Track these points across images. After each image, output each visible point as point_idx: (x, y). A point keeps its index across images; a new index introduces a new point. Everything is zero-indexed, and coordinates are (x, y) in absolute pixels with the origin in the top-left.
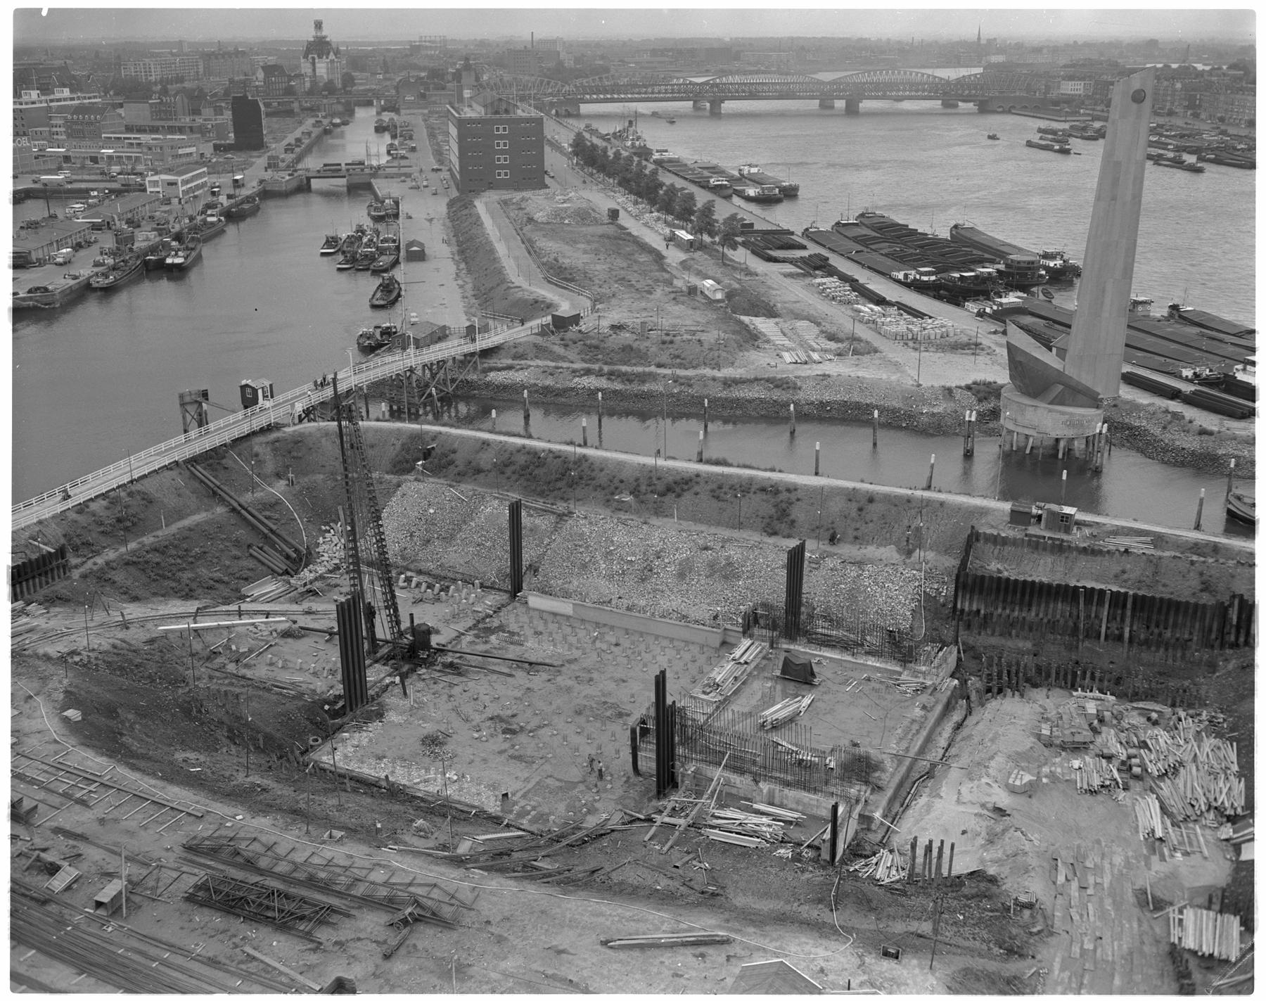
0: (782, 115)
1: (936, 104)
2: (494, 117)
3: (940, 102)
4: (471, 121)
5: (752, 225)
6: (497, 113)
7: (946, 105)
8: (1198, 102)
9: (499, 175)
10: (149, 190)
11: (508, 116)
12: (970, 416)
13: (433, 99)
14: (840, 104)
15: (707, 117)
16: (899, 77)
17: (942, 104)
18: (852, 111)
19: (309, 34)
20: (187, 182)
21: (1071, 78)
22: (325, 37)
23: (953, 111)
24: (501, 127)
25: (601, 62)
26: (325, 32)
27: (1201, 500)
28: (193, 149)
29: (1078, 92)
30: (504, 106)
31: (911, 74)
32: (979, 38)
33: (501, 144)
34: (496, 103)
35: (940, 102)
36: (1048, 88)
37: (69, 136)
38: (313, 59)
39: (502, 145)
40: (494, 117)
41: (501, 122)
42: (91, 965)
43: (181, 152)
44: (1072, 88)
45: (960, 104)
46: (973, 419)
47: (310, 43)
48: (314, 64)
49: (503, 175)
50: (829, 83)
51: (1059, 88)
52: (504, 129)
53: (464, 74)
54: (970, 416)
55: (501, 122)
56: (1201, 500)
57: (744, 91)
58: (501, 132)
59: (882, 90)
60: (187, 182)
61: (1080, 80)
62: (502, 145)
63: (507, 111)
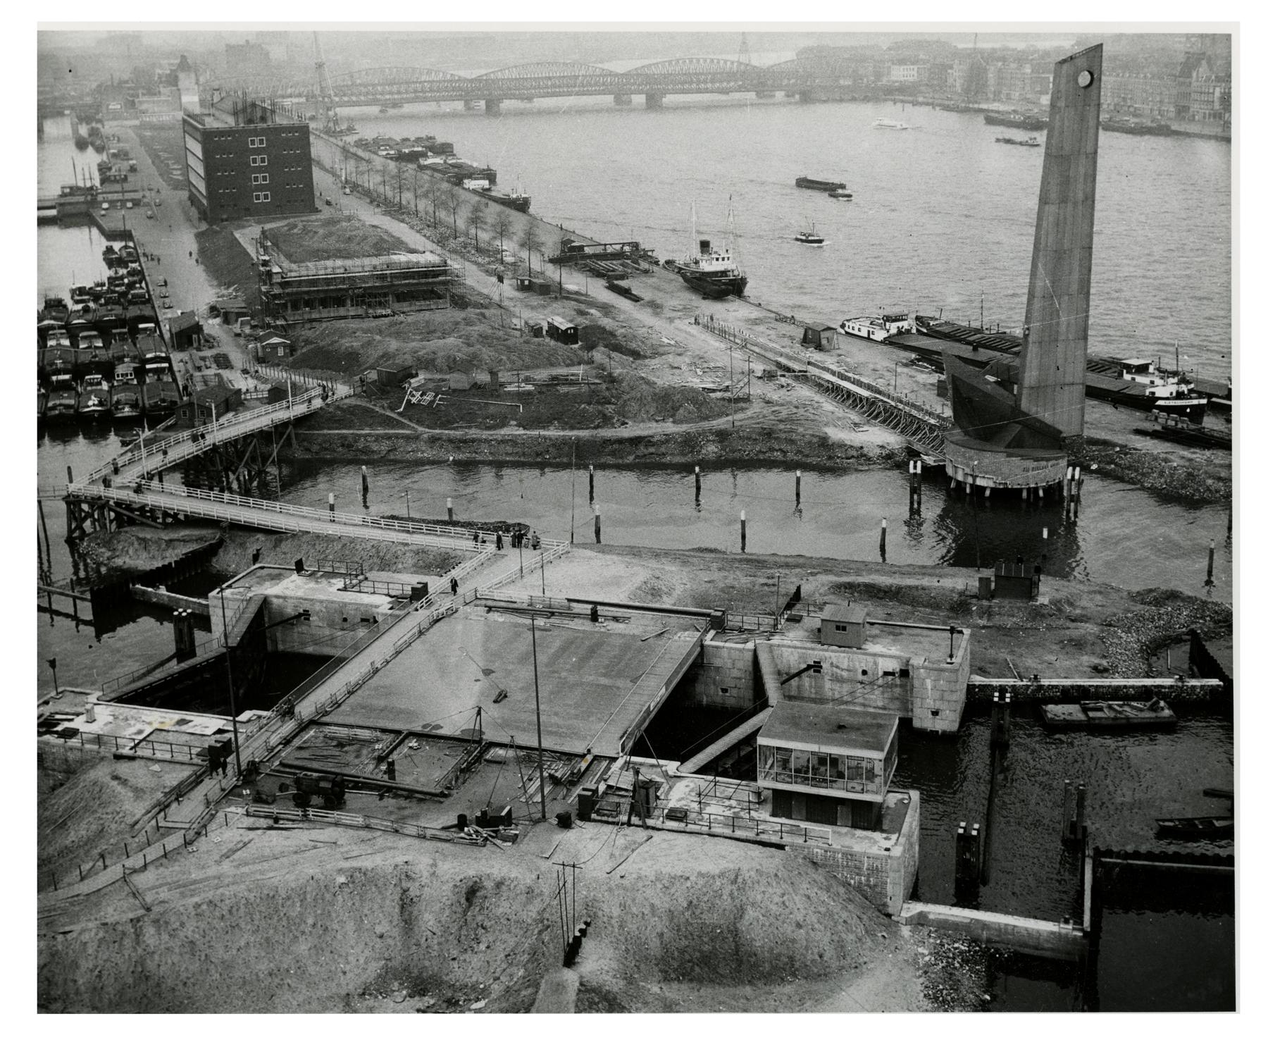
0: (581, 111)
4: (221, 133)
5: (581, 248)
6: (250, 121)
7: (618, 100)
11: (265, 125)
12: (915, 467)
13: (144, 107)
14: (639, 99)
15: (796, 103)
16: (692, 67)
18: (653, 103)
21: (902, 62)
23: (772, 101)
27: (884, 531)
31: (718, 63)
33: (258, 160)
34: (249, 110)
36: (878, 76)
39: (258, 161)
41: (256, 133)
44: (902, 74)
46: (919, 471)
49: (262, 198)
50: (472, 81)
51: (889, 73)
52: (261, 141)
53: (182, 76)
54: (915, 467)
55: (256, 133)
56: (884, 531)
57: (596, 84)
61: (913, 64)
63: (263, 119)
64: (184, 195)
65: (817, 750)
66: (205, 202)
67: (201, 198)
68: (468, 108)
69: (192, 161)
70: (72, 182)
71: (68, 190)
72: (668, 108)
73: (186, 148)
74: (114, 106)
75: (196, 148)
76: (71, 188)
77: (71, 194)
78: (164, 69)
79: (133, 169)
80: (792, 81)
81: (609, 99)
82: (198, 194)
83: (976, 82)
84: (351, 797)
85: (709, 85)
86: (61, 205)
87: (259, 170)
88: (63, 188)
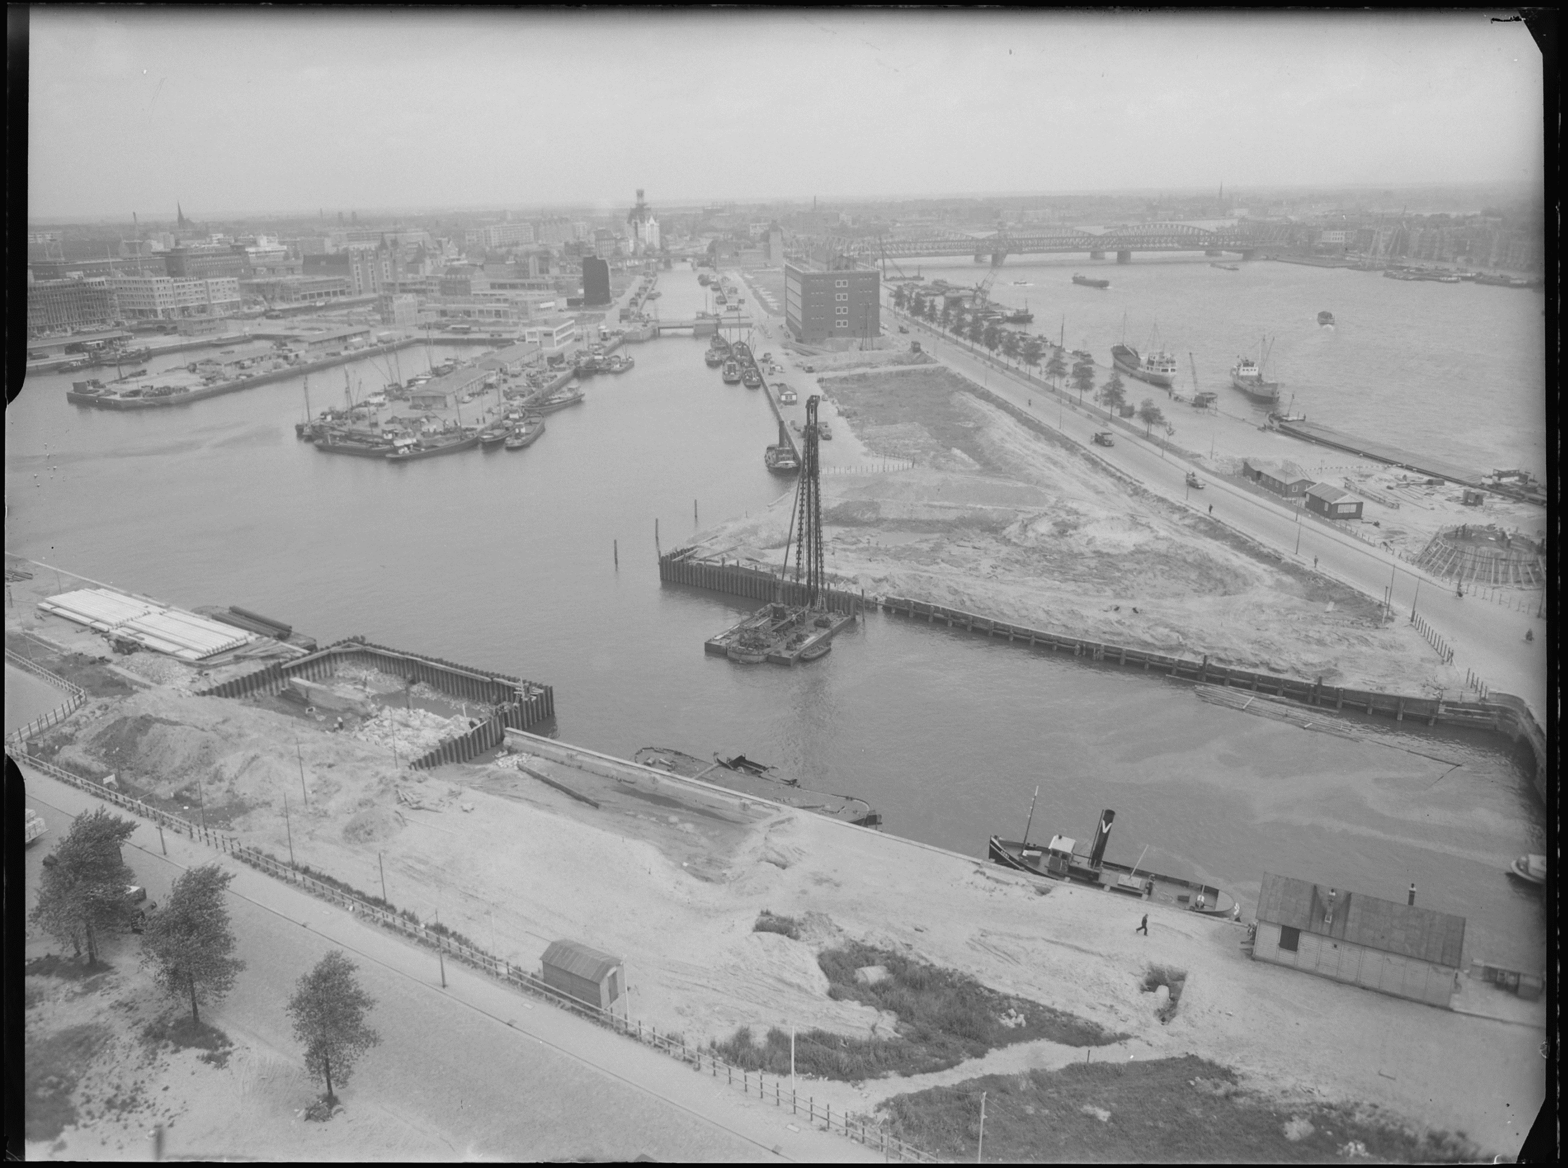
1: (970, 259)
2: (835, 272)
3: (1204, 252)
4: (814, 276)
6: (838, 268)
8: (1468, 248)
9: (839, 324)
10: (528, 340)
11: (848, 271)
14: (1112, 256)
17: (1206, 254)
19: (631, 201)
20: (562, 331)
21: (1333, 227)
22: (645, 204)
24: (841, 281)
25: (876, 222)
26: (647, 198)
28: (552, 304)
29: (1339, 241)
30: (844, 262)
32: (1221, 194)
35: (1204, 252)
37: (444, 293)
38: (636, 224)
39: (841, 297)
40: (835, 272)
42: (628, 789)
43: (542, 306)
44: (1336, 237)
45: (1224, 253)
47: (633, 210)
48: (636, 228)
57: (1066, 244)
58: (842, 285)
59: (1143, 242)
60: (562, 331)
61: (1342, 229)
62: (841, 297)
63: (847, 267)
64: (782, 321)
65: (1093, 1049)
66: (800, 327)
67: (796, 323)
68: (977, 259)
69: (791, 296)
70: (702, 308)
71: (700, 315)
72: (1134, 264)
73: (787, 287)
74: (725, 256)
75: (798, 288)
76: (703, 314)
77: (703, 318)
78: (756, 230)
79: (741, 301)
80: (1239, 243)
81: (970, 259)
82: (794, 321)
83: (1400, 245)
84: (532, 965)
85: (907, 252)
86: (697, 325)
87: (842, 303)
88: (697, 313)
